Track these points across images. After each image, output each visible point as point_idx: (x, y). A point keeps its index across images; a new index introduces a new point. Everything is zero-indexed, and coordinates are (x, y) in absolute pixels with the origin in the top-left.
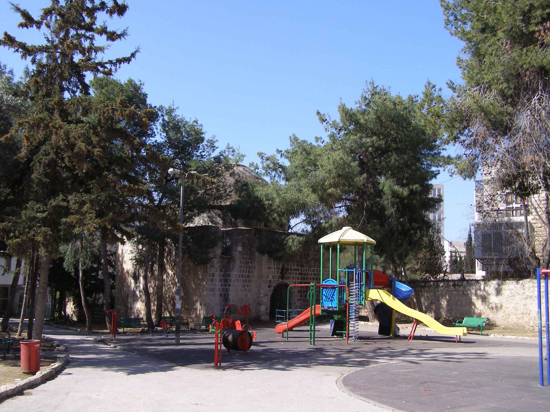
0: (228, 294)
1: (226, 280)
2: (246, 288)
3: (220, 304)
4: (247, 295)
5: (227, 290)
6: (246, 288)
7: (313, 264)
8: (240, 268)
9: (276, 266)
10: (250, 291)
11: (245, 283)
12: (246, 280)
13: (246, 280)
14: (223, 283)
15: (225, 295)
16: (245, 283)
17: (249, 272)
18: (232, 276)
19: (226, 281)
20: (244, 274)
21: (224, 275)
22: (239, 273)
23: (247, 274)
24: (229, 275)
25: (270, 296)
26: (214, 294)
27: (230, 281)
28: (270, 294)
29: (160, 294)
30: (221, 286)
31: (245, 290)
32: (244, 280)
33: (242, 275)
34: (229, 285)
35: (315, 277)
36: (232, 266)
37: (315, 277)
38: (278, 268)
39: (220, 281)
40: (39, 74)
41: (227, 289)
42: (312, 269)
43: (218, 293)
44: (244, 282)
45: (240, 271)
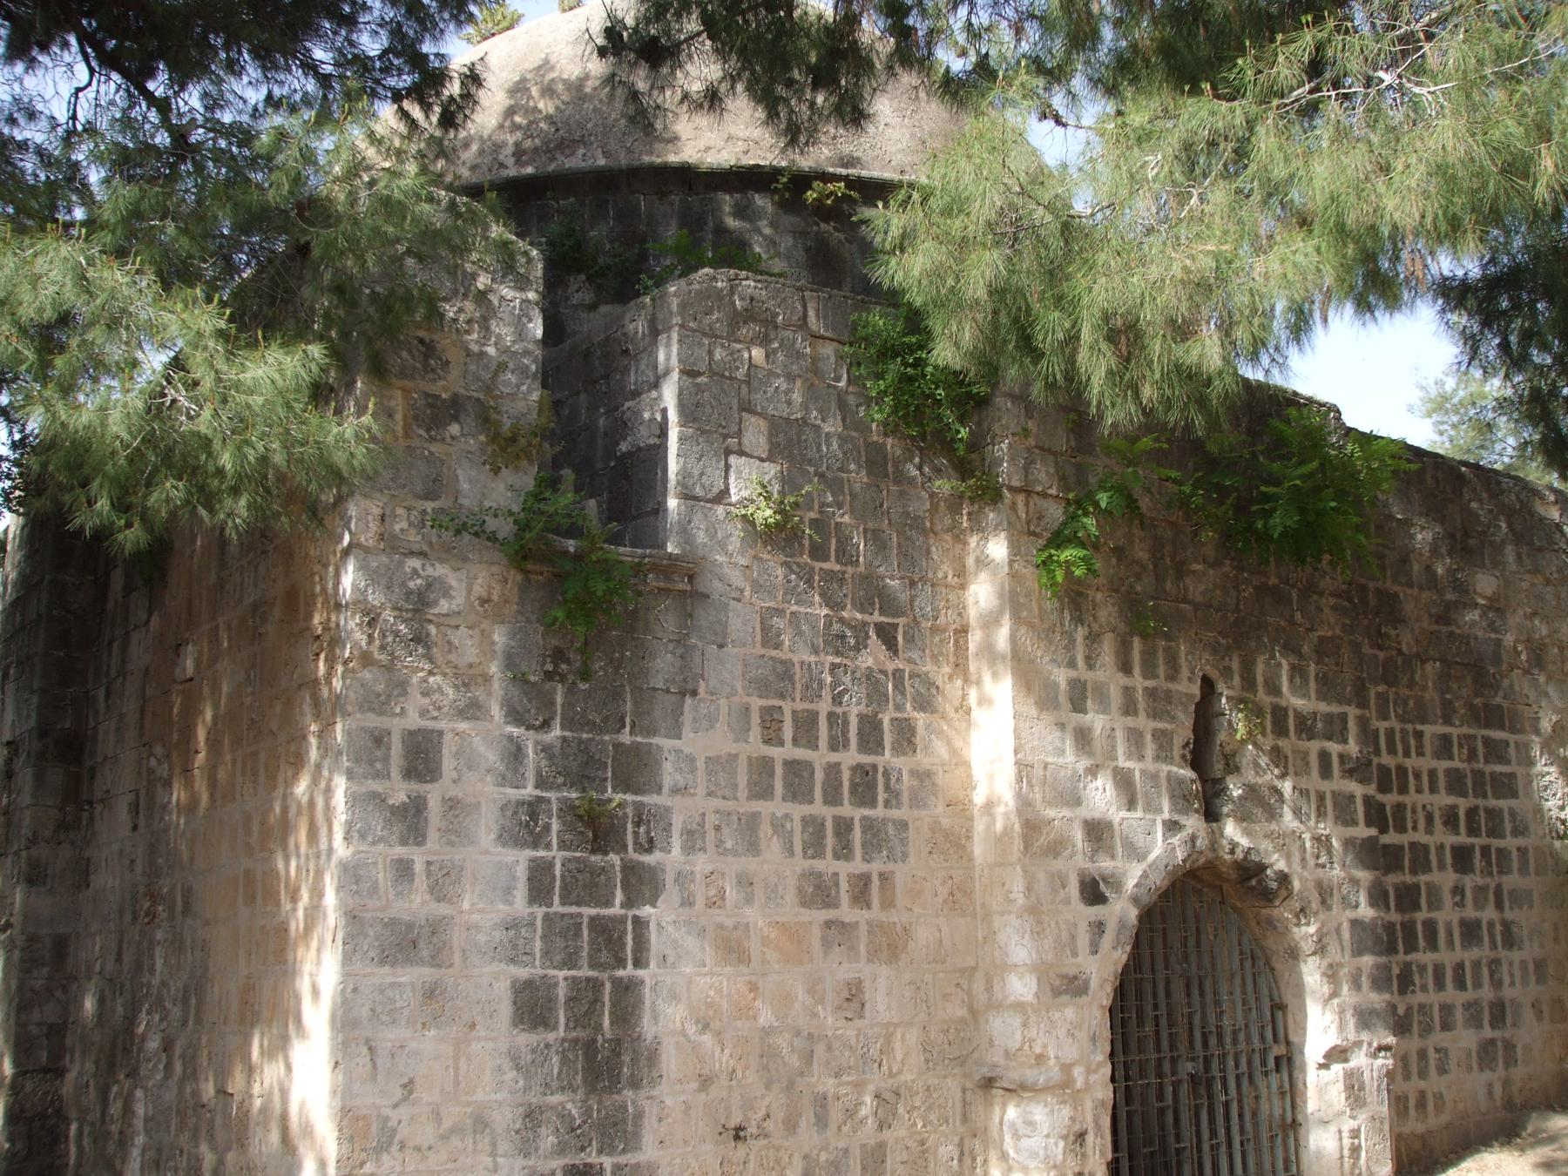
0: (627, 991)
1: (594, 832)
2: (846, 912)
3: (532, 1116)
4: (854, 997)
5: (615, 943)
6: (846, 912)
7: (1431, 694)
8: (761, 687)
9: (1139, 682)
10: (890, 946)
11: (827, 865)
12: (843, 827)
13: (843, 827)
14: (557, 856)
15: (585, 997)
16: (827, 865)
17: (871, 736)
18: (669, 774)
19: (596, 828)
20: (820, 757)
21: (577, 766)
22: (754, 744)
23: (851, 757)
24: (636, 769)
25: (1101, 994)
26: (431, 992)
27: (651, 835)
28: (1102, 968)
29: (50, 1012)
30: (539, 887)
31: (838, 932)
32: (814, 827)
33: (797, 772)
34: (642, 884)
35: (1463, 804)
36: (663, 665)
37: (1463, 804)
38: (1159, 703)
39: (525, 825)
40: (473, 677)
41: (608, 936)
42: (1428, 729)
43: (494, 983)
44: (814, 846)
45: (771, 721)
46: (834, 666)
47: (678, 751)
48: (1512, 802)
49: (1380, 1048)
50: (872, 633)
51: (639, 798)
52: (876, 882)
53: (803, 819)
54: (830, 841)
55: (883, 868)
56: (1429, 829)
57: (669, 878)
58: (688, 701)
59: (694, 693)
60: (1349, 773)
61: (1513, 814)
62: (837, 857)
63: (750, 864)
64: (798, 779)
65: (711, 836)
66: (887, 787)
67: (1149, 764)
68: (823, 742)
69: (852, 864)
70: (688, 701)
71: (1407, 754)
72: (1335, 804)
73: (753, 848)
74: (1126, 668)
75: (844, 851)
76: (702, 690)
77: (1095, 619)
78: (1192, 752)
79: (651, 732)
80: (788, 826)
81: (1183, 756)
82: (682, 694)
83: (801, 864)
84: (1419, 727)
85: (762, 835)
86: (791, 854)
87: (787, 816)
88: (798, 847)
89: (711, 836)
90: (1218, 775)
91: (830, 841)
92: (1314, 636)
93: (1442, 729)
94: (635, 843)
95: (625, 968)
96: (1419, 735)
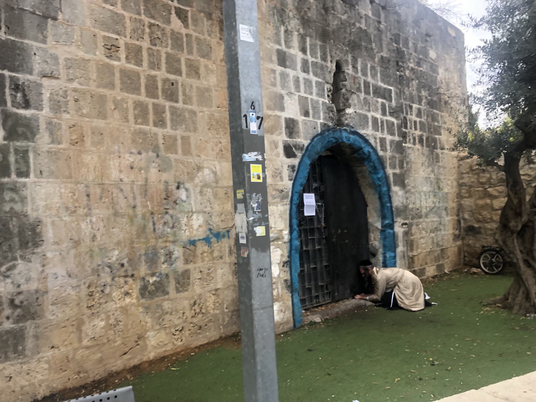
18: (37, 64)
20: (144, 70)
23: (162, 74)
45: (111, 49)
46: (151, 25)
47: (44, 50)
48: (440, 137)
49: (403, 224)
50: (173, 12)
51: (13, 74)
52: (179, 142)
53: (135, 102)
54: (151, 117)
55: (186, 134)
56: (414, 144)
57: (43, 126)
58: (50, 22)
59: (55, 19)
60: (391, 114)
61: (440, 139)
62: (155, 125)
63: (100, 123)
64: (130, 82)
65: (72, 103)
66: (184, 94)
67: (315, 97)
68: (145, 64)
69: (166, 130)
70: (50, 22)
71: (407, 114)
72: (387, 125)
73: (103, 115)
74: (303, 50)
75: (160, 122)
76: (60, 17)
77: (289, 24)
78: (332, 94)
79: (22, 35)
80: (125, 106)
81: (328, 96)
82: (45, 17)
83: (134, 127)
84: (411, 104)
85: (108, 108)
86: (127, 120)
87: (123, 100)
88: (131, 118)
89: (72, 103)
90: (342, 108)
91: (151, 117)
92: (380, 54)
93: (418, 106)
94: (13, 102)
95: (9, 176)
96: (411, 107)
